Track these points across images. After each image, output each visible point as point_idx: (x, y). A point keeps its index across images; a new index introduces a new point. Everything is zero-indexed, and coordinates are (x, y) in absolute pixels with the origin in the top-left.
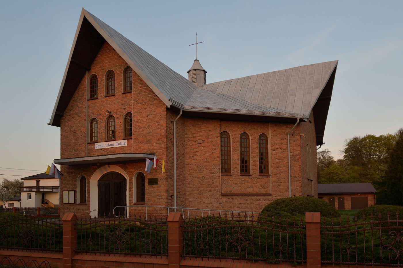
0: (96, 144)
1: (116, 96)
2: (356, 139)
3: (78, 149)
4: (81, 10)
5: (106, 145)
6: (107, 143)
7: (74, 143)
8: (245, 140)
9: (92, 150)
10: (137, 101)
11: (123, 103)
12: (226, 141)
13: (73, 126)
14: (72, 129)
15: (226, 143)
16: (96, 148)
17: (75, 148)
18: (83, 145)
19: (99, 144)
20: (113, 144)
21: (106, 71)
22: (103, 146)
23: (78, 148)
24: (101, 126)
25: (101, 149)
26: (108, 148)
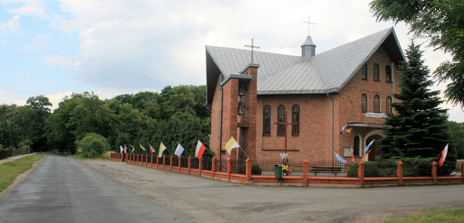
0: (367, 113)
1: (381, 83)
2: (14, 105)
3: (354, 115)
4: (392, 27)
5: (375, 115)
6: (375, 114)
7: (351, 109)
8: (269, 110)
9: (363, 117)
10: (397, 90)
11: (386, 88)
12: (283, 111)
13: (350, 96)
14: (349, 98)
15: (283, 113)
16: (367, 116)
17: (352, 113)
18: (359, 112)
19: (369, 113)
20: (379, 116)
21: (374, 62)
22: (372, 115)
23: (355, 114)
24: (370, 101)
25: (371, 117)
26: (376, 118)
